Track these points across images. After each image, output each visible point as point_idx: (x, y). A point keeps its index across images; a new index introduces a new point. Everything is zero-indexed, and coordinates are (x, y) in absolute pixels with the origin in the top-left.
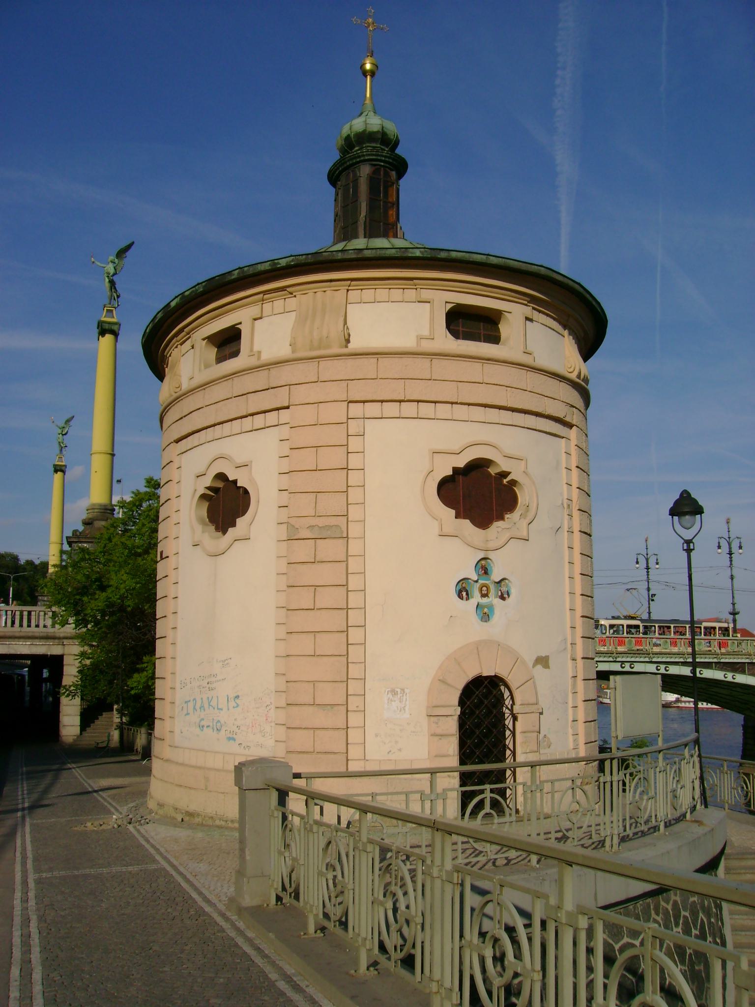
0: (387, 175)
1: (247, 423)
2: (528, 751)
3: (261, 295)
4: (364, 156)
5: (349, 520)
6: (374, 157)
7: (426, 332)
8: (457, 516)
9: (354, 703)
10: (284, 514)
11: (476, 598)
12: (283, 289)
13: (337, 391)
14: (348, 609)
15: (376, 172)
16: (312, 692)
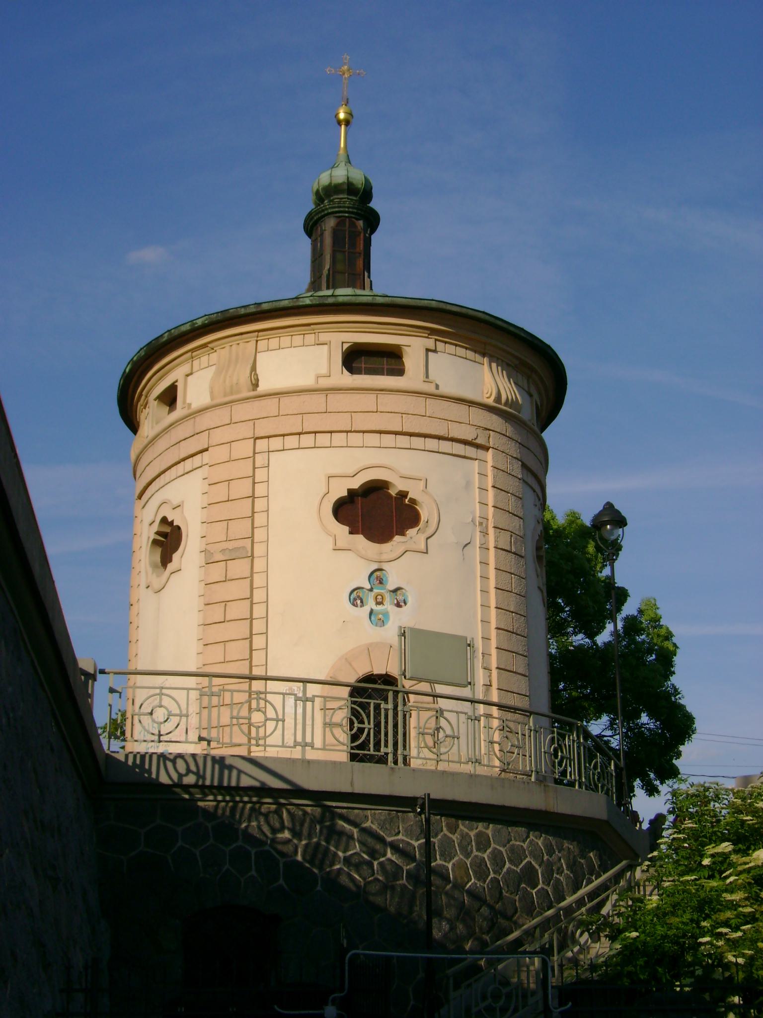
0: (353, 225)
1: (180, 468)
3: (190, 354)
4: (327, 209)
6: (337, 210)
7: (324, 371)
8: (351, 533)
11: (371, 604)
12: (205, 346)
13: (245, 430)
15: (341, 223)
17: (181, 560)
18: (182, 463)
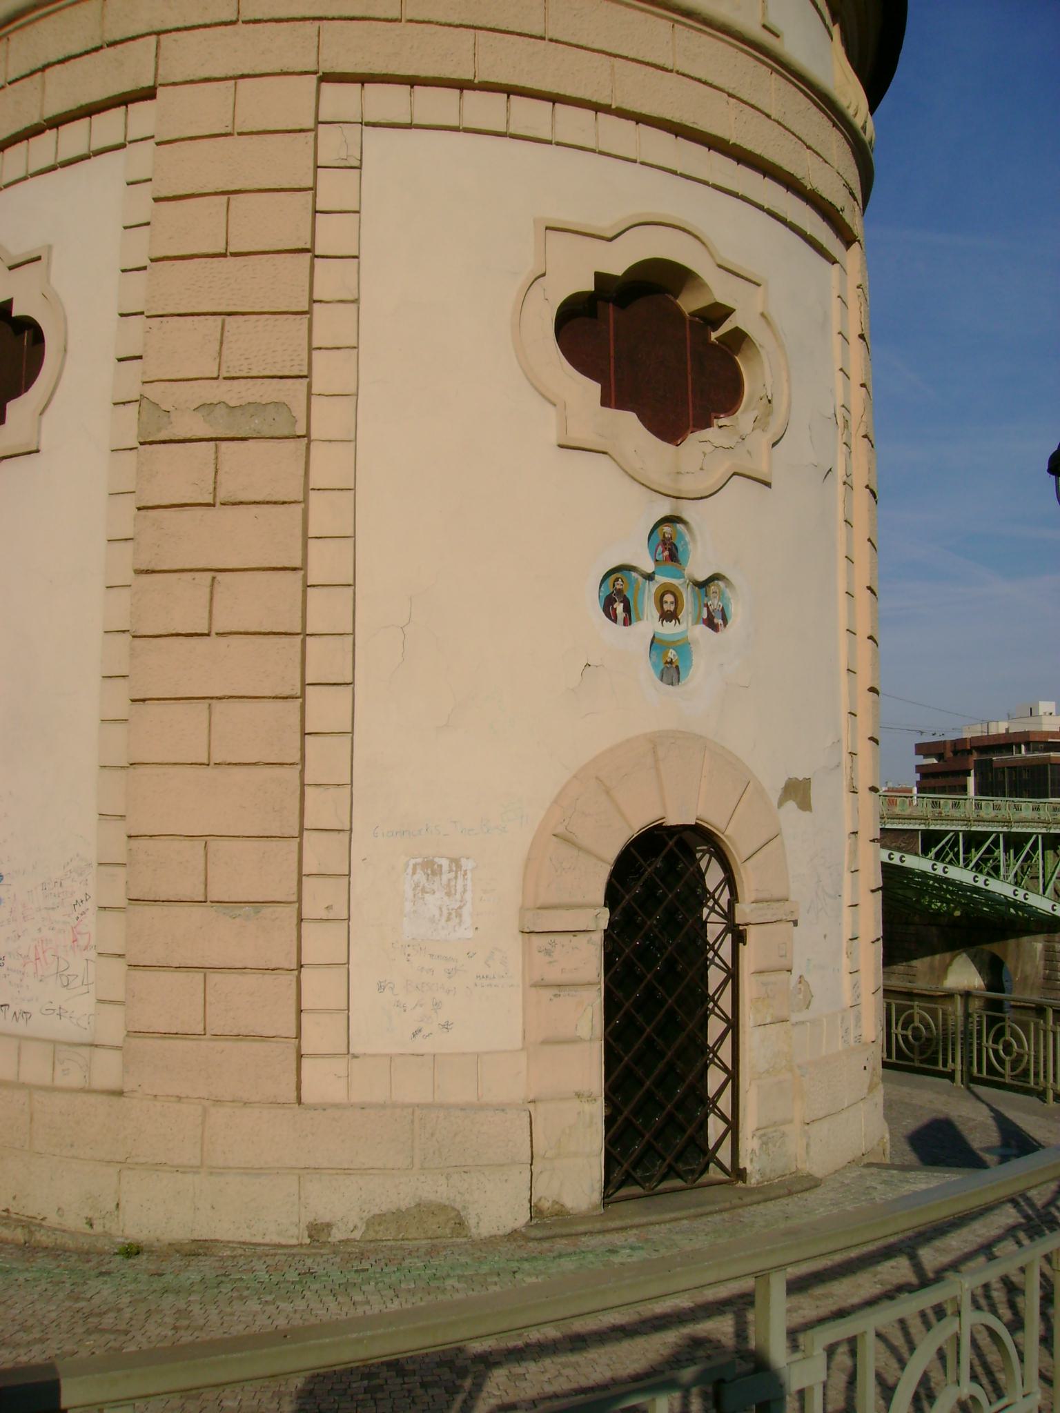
2: (768, 1021)
5: (315, 390)
8: (605, 402)
9: (317, 899)
10: (131, 380)
11: (649, 623)
14: (306, 635)
16: (202, 866)
17: (40, 422)
18: (50, 135)
